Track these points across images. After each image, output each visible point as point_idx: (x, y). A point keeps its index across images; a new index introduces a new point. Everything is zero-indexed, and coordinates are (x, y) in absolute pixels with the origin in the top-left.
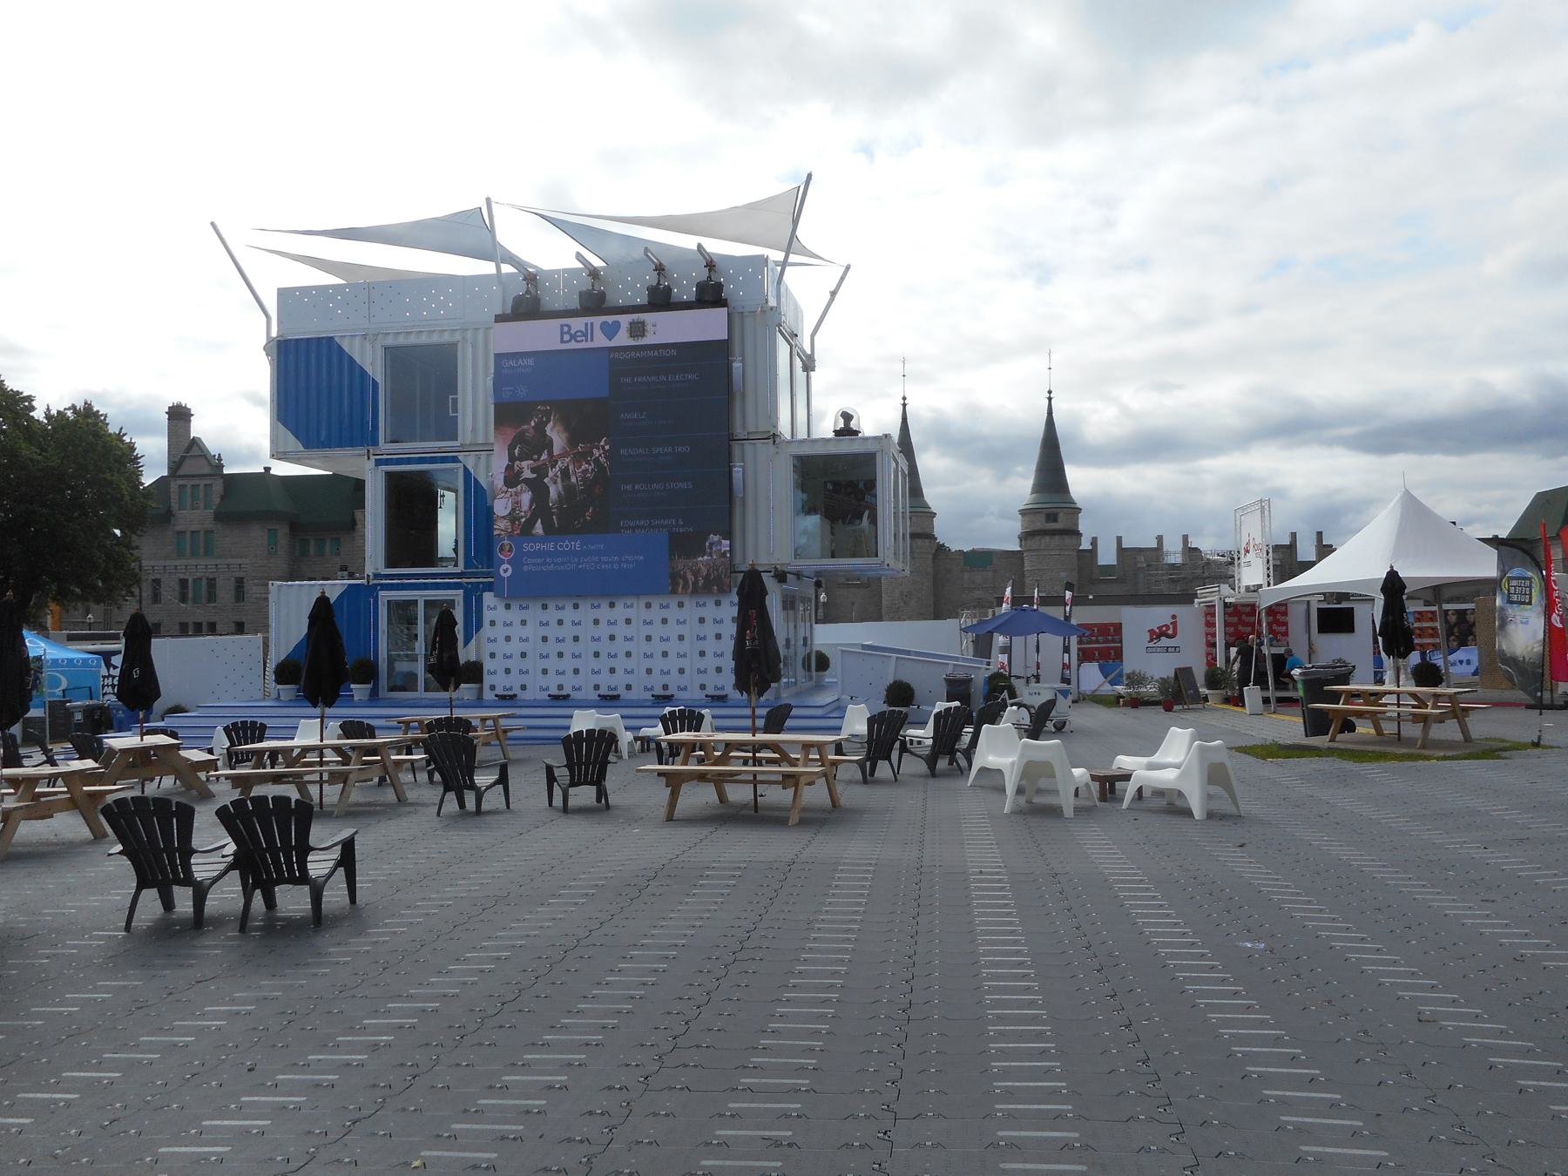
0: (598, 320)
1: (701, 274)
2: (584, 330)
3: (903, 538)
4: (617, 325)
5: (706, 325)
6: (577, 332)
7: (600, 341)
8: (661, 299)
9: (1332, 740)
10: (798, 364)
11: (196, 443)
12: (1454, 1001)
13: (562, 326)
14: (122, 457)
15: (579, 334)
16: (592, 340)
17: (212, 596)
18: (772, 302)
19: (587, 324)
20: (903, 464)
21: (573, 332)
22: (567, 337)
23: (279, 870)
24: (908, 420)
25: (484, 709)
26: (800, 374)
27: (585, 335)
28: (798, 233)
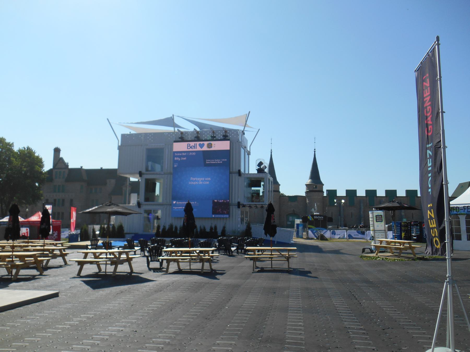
0: (198, 143)
1: (223, 133)
2: (194, 146)
3: (271, 192)
4: (203, 144)
5: (224, 146)
6: (192, 146)
7: (198, 149)
8: (214, 138)
9: (377, 255)
10: (246, 153)
11: (62, 159)
12: (430, 338)
13: (188, 144)
14: (39, 162)
15: (193, 146)
16: (196, 148)
17: (63, 205)
18: (240, 140)
19: (195, 144)
20: (271, 179)
21: (191, 146)
22: (189, 147)
23: (233, 242)
24: (272, 157)
25: (448, 211)
26: (247, 156)
27: (194, 147)
28: (247, 123)
